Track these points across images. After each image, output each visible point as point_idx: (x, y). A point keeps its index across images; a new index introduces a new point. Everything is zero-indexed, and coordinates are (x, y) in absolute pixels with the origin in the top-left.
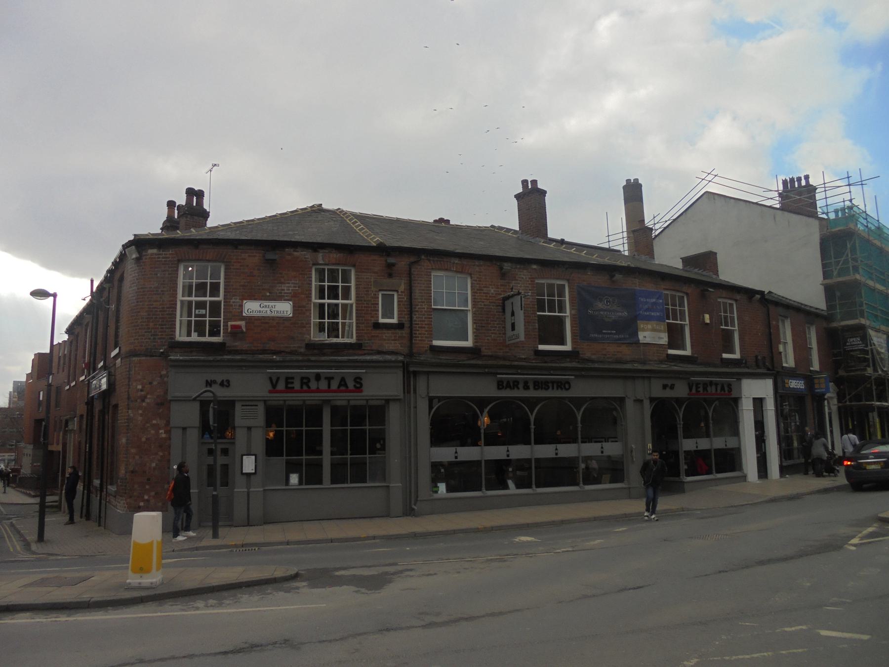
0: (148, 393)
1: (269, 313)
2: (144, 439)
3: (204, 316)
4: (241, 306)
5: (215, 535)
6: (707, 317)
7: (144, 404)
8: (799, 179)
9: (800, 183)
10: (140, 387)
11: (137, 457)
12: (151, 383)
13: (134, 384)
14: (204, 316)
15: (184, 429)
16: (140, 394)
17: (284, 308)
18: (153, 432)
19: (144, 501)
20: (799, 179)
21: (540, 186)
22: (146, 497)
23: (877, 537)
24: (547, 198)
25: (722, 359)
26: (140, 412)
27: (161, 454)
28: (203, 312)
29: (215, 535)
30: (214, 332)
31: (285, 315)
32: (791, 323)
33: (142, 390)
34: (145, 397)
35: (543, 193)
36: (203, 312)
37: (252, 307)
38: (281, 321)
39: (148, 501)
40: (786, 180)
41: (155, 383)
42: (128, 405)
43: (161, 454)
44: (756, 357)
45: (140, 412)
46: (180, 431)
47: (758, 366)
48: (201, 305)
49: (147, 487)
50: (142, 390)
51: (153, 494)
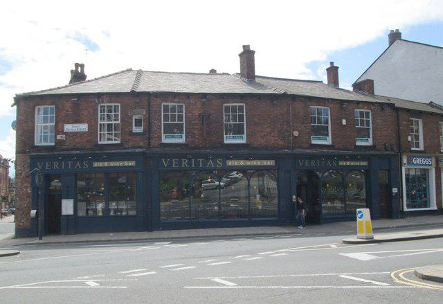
1: (76, 130)
17: (83, 127)
24: (256, 56)
36: (46, 131)
38: (83, 133)
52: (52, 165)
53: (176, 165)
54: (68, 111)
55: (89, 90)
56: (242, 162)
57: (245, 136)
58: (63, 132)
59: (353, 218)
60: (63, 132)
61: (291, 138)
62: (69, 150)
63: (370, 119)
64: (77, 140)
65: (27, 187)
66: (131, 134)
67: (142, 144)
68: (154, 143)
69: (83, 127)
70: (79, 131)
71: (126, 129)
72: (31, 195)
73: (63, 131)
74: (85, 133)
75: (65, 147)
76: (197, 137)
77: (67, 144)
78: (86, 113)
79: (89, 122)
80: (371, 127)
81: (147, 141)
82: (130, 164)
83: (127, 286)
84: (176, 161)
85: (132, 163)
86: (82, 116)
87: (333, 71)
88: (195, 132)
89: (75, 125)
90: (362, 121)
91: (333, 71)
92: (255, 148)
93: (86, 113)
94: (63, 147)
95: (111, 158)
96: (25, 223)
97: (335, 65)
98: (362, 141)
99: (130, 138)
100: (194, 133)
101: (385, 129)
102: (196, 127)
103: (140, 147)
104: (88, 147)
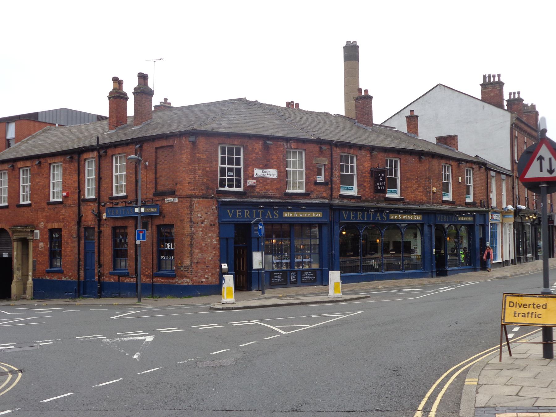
0: (205, 219)
1: (266, 176)
2: (204, 245)
3: (232, 176)
4: (253, 171)
5: (263, 293)
6: (460, 178)
7: (203, 225)
8: (494, 76)
9: (494, 79)
10: (200, 215)
11: (200, 254)
12: (206, 213)
13: (196, 213)
14: (232, 176)
15: (227, 239)
16: (199, 219)
17: (273, 173)
18: (209, 240)
19: (205, 278)
20: (494, 76)
21: (370, 94)
22: (206, 276)
23: (446, 376)
24: (373, 101)
25: (466, 203)
26: (201, 229)
27: (214, 252)
28: (231, 174)
29: (263, 293)
30: (239, 186)
31: (274, 177)
32: (496, 181)
33: (201, 217)
34: (204, 221)
35: (371, 98)
36: (231, 174)
37: (259, 172)
38: (272, 180)
39: (207, 278)
40: (486, 75)
41: (209, 213)
42: (191, 225)
43: (214, 252)
44: (481, 201)
45: (201, 229)
46: (256, 239)
47: (481, 206)
48: (230, 170)
49: (207, 271)
50: (201, 217)
51: (210, 274)
52: (243, 214)
53: (239, 215)
54: (257, 154)
55: (426, 148)
56: (295, 213)
57: (399, 190)
58: (253, 178)
59: (324, 280)
60: (253, 178)
61: (431, 194)
62: (260, 197)
63: (355, 165)
64: (267, 187)
65: (211, 238)
66: (316, 184)
67: (325, 195)
68: (335, 195)
69: (273, 173)
70: (269, 176)
71: (312, 179)
72: (218, 246)
73: (253, 175)
74: (274, 179)
75: (256, 194)
76: (367, 190)
77: (258, 190)
78: (275, 157)
79: (278, 168)
80: (355, 173)
81: (329, 192)
82: (317, 215)
83: (179, 364)
84: (239, 212)
85: (318, 215)
86: (272, 161)
87: (412, 120)
88: (365, 184)
89: (265, 170)
90: (347, 167)
91: (412, 120)
92: (408, 203)
93: (275, 157)
94: (253, 194)
95: (297, 207)
96: (210, 278)
97: (415, 113)
98: (346, 188)
99: (315, 187)
100: (365, 186)
101: (166, 162)
102: (367, 180)
103: (324, 198)
104: (278, 195)
